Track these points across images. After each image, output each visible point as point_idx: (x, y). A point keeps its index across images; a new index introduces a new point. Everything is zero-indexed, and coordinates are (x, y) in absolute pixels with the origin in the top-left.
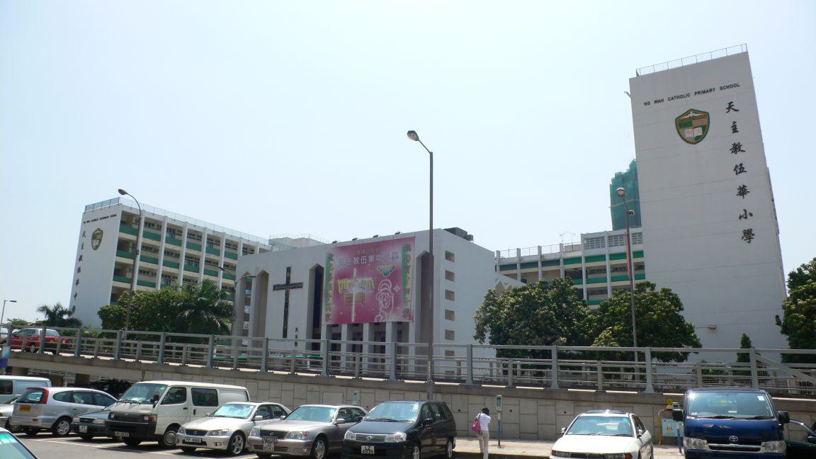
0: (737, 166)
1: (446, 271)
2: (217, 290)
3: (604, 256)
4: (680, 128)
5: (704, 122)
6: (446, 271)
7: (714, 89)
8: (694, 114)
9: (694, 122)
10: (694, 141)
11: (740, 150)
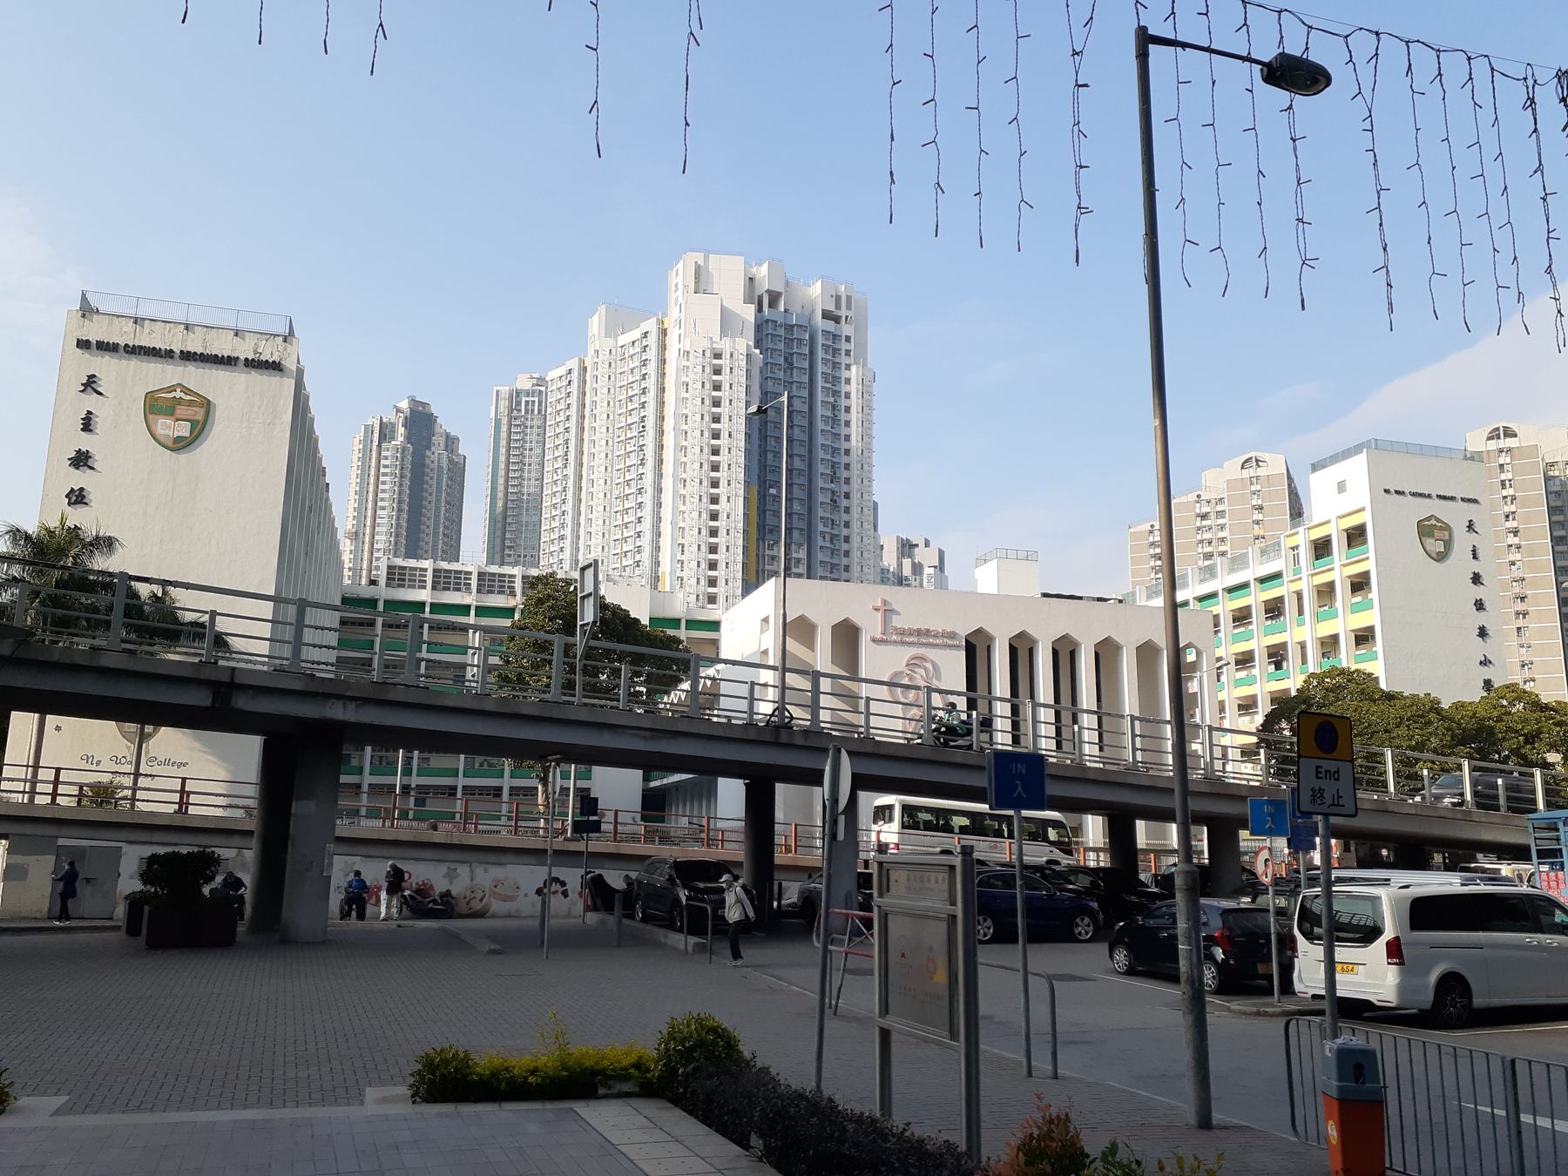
0: (72, 490)
1: (1339, 493)
2: (959, 1150)
3: (469, 607)
4: (152, 413)
5: (199, 414)
6: (1339, 493)
7: (1474, 546)
8: (182, 395)
9: (181, 411)
10: (170, 444)
11: (86, 465)
